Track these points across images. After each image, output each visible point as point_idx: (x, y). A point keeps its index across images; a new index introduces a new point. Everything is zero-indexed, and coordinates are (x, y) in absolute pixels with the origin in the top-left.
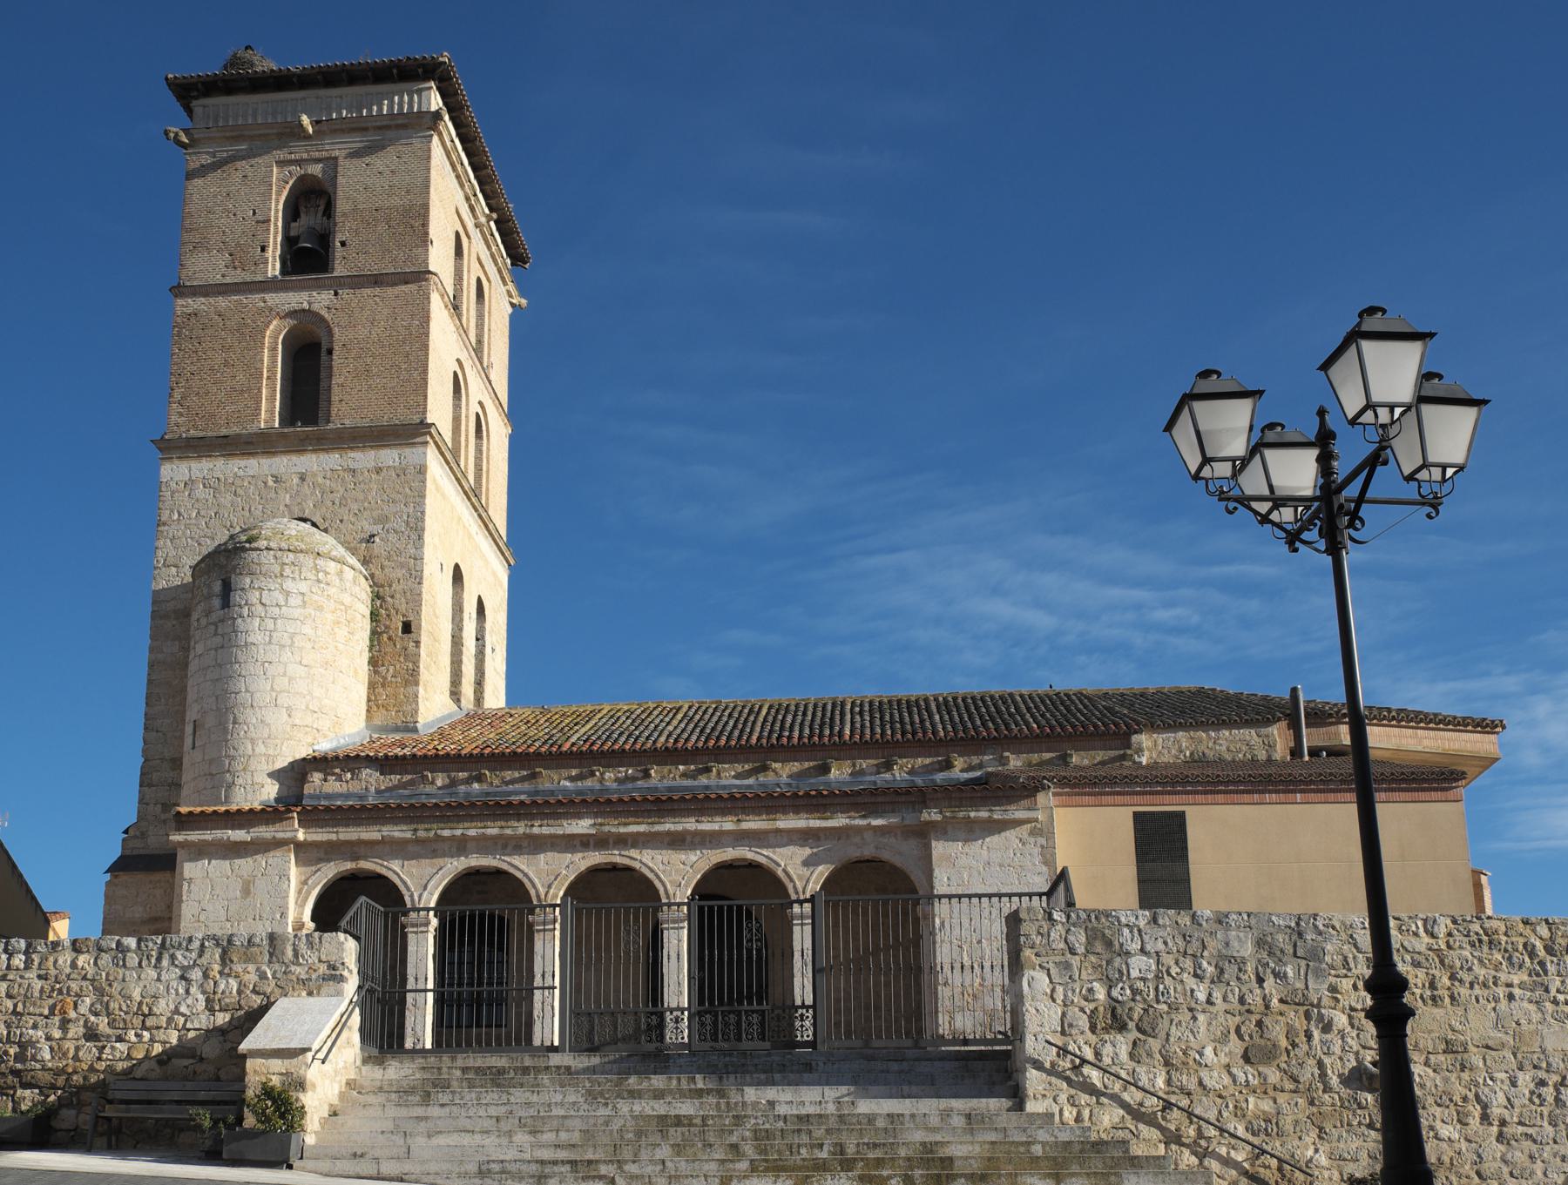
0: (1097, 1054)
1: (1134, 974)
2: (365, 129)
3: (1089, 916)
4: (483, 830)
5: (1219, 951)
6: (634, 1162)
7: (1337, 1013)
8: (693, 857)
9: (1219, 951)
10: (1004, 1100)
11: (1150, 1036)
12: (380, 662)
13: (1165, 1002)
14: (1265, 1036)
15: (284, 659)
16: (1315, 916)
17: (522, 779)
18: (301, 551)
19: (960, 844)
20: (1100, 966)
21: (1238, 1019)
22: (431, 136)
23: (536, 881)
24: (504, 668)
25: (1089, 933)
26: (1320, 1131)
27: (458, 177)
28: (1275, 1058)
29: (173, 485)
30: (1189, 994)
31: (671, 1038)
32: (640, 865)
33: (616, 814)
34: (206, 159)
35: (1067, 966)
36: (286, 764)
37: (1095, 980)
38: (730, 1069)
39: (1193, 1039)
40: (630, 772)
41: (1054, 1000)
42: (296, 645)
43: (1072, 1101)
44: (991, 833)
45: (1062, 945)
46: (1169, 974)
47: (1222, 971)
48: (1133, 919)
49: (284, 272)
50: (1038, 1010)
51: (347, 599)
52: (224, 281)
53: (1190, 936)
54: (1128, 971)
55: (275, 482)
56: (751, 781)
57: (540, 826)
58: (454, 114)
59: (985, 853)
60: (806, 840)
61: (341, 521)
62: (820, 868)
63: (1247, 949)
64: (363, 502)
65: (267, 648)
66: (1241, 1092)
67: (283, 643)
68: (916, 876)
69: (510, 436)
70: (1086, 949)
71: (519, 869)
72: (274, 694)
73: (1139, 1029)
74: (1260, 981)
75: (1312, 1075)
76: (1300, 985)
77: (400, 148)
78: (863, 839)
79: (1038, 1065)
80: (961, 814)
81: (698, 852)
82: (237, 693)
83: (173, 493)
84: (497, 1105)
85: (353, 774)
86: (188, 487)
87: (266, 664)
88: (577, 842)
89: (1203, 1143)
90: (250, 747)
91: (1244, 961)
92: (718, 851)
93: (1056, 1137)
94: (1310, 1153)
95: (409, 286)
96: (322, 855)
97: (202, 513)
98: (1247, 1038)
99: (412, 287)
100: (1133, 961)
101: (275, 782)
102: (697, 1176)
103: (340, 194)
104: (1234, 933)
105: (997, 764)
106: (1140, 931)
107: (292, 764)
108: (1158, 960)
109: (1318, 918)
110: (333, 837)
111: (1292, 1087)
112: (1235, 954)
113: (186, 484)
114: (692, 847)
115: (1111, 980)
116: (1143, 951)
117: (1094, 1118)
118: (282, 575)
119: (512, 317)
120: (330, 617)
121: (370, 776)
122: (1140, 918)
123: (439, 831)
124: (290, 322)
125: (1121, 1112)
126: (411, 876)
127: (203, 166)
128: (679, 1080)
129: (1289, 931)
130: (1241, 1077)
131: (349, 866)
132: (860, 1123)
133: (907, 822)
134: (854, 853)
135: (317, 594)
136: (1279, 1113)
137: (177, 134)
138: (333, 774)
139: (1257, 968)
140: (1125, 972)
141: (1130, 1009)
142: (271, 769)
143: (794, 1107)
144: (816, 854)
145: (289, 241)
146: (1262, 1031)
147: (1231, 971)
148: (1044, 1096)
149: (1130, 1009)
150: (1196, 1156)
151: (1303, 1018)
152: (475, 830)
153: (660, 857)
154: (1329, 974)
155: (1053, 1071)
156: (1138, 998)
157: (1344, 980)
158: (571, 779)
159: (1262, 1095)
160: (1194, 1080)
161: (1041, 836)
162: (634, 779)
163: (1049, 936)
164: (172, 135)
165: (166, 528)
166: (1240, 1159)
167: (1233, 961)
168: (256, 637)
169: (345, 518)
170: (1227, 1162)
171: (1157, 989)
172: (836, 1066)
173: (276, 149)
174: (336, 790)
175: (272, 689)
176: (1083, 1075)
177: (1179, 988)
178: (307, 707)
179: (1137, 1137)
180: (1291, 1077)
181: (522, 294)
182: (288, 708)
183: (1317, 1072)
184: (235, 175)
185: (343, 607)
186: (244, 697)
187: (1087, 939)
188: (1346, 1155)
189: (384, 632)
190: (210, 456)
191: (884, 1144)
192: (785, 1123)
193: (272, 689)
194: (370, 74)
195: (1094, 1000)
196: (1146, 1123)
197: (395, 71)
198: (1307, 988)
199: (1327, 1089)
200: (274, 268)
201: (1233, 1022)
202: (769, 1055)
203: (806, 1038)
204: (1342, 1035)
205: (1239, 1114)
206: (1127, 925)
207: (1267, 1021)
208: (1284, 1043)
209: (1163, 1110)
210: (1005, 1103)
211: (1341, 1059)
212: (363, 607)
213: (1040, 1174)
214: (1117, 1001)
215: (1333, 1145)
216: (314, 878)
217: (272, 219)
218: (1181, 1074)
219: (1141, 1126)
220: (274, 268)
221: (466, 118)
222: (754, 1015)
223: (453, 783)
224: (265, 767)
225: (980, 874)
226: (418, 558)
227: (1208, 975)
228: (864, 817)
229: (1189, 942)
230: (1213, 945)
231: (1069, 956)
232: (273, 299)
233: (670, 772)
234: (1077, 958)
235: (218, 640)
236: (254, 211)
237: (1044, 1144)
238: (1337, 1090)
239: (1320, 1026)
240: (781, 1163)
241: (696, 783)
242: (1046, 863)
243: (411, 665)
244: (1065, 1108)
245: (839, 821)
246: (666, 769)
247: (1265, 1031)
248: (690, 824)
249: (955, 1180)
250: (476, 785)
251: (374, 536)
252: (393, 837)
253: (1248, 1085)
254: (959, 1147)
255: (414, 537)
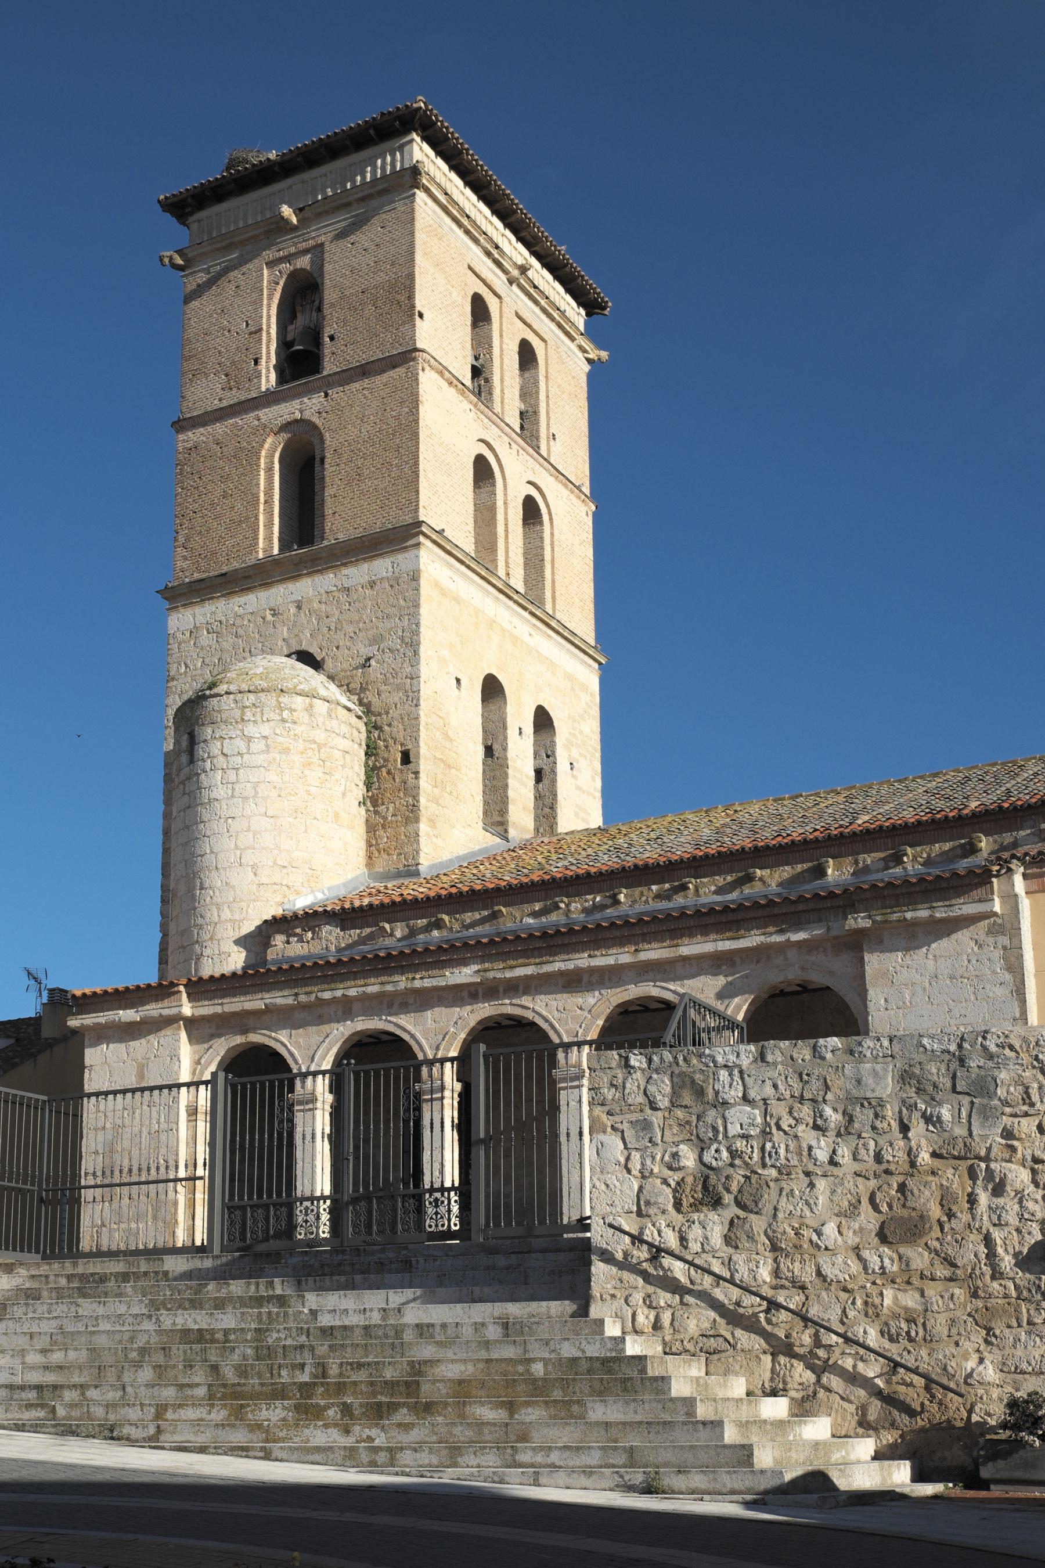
0: (683, 1240)
1: (734, 1129)
2: (348, 205)
3: (675, 1058)
4: (364, 989)
5: (848, 1092)
6: (96, 1387)
7: (1013, 1166)
8: (591, 999)
9: (848, 1092)
10: (567, 1302)
11: (751, 1212)
12: (380, 801)
13: (773, 1166)
14: (909, 1204)
15: (248, 812)
16: (984, 1035)
17: (483, 921)
18: (263, 690)
19: (900, 954)
20: (688, 1123)
21: (873, 1183)
22: (414, 194)
23: (424, 1042)
24: (598, 783)
25: (675, 1080)
26: (988, 1334)
27: (467, 232)
28: (921, 1236)
29: (179, 635)
30: (805, 1153)
31: (430, 1226)
32: (533, 1014)
33: (503, 956)
34: (202, 278)
35: (646, 1125)
36: (253, 928)
37: (682, 1141)
38: (327, 1269)
39: (808, 1213)
40: (598, 899)
41: (629, 1171)
42: (260, 795)
43: (649, 1302)
44: (938, 937)
45: (641, 1099)
46: (779, 1128)
47: (850, 1119)
48: (732, 1058)
49: (281, 379)
50: (607, 1186)
51: (320, 736)
52: (221, 406)
53: (808, 1075)
54: (725, 1128)
55: (273, 615)
56: (734, 895)
57: (421, 978)
58: (454, 163)
59: (930, 963)
60: (719, 967)
61: (337, 648)
62: (736, 1000)
63: (887, 1087)
64: (358, 622)
65: (231, 802)
66: (874, 1283)
67: (246, 794)
68: (851, 998)
69: (594, 514)
70: (671, 1102)
71: (405, 1030)
72: (238, 852)
73: (739, 1204)
74: (904, 1128)
75: (976, 1255)
76: (960, 1131)
77: (384, 216)
78: (786, 959)
79: (607, 1257)
80: (895, 917)
81: (597, 993)
82: (202, 856)
83: (180, 644)
84: (49, 1319)
85: (313, 933)
86: (193, 635)
87: (230, 820)
88: (465, 994)
89: (821, 1353)
90: (216, 914)
91: (881, 1103)
92: (619, 990)
93: (583, 1351)
94: (971, 1364)
95: (397, 370)
96: (213, 1031)
97: (207, 661)
98: (884, 1208)
99: (400, 371)
100: (731, 1113)
101: (241, 949)
102: (134, 1405)
103: (327, 282)
104: (868, 1066)
105: (1037, 839)
106: (741, 1072)
107: (259, 927)
108: (766, 1110)
109: (989, 1036)
110: (218, 1009)
111: (947, 1273)
112: (869, 1095)
113: (191, 632)
114: (590, 987)
115: (702, 1141)
116: (745, 1099)
117: (676, 1324)
118: (243, 720)
119: (590, 376)
120: (298, 759)
121: (330, 934)
122: (743, 1056)
123: (320, 994)
124: (285, 436)
125: (712, 1314)
126: (299, 1047)
127: (199, 286)
128: (257, 1285)
129: (947, 1057)
130: (874, 1262)
131: (239, 1040)
132: (386, 1336)
133: (834, 933)
134: (776, 976)
135: (282, 735)
136: (926, 1310)
137: (171, 258)
138: (296, 935)
139: (900, 1112)
140: (721, 1129)
141: (727, 1178)
142: (237, 935)
143: (337, 1318)
144: (731, 983)
145: (284, 344)
146: (906, 1199)
147: (863, 1117)
148: (613, 1296)
149: (727, 1178)
150: (814, 1372)
151: (966, 1176)
152: (355, 989)
153: (555, 1003)
154: (1003, 1113)
155: (626, 1265)
156: (737, 1162)
157: (1024, 1121)
158: (535, 914)
159: (904, 1286)
160: (811, 1269)
161: (1003, 934)
162: (602, 907)
163: (624, 1087)
164: (166, 261)
165: (175, 683)
166: (871, 1374)
167: (866, 1104)
168: (220, 792)
169: (341, 644)
170: (853, 1378)
171: (763, 1149)
172: (438, 1263)
173: (265, 250)
174: (298, 953)
175: (236, 847)
176: (663, 1268)
177: (792, 1146)
178: (275, 863)
179: (734, 1347)
180: (945, 1259)
181: (600, 346)
182: (253, 866)
183: (983, 1250)
184: (227, 288)
185: (314, 746)
186: (209, 860)
187: (673, 1087)
188: (1024, 1366)
189: (383, 766)
190: (212, 598)
191: (369, 1364)
192: (308, 1336)
193: (236, 847)
194: (348, 142)
195: (680, 1169)
196: (747, 1329)
197: (372, 132)
198: (971, 1134)
199: (997, 1275)
200: (268, 381)
201: (864, 1187)
202: (383, 1251)
203: (441, 1229)
204: (1020, 1197)
205: (870, 1312)
206: (726, 1066)
207: (911, 1183)
208: (936, 1212)
209: (767, 1311)
210: (568, 1307)
211: (1018, 1231)
212: (346, 744)
213: (490, 1402)
214: (710, 1168)
215: (1007, 1351)
216: (206, 1056)
217: (264, 327)
218: (793, 1261)
219: (739, 1333)
220: (268, 381)
221: (470, 162)
222: (259, 1211)
223: (413, 933)
224: (231, 933)
225: (924, 990)
226: (414, 677)
227: (832, 1125)
228: (781, 931)
229: (807, 1082)
230: (839, 1085)
231: (648, 1111)
232: (269, 414)
233: (642, 894)
234: (660, 1114)
235: (186, 799)
236: (247, 322)
237: (546, 1362)
238: (1011, 1275)
239: (990, 1187)
240: (238, 1389)
241: (671, 905)
242: (1009, 969)
243: (410, 800)
244: (639, 1311)
245: (753, 939)
246: (637, 891)
247: (909, 1199)
248: (582, 960)
249: (397, 1410)
250: (435, 933)
251: (369, 659)
252: (275, 1005)
253: (884, 1273)
254: (451, 1366)
255: (409, 653)
